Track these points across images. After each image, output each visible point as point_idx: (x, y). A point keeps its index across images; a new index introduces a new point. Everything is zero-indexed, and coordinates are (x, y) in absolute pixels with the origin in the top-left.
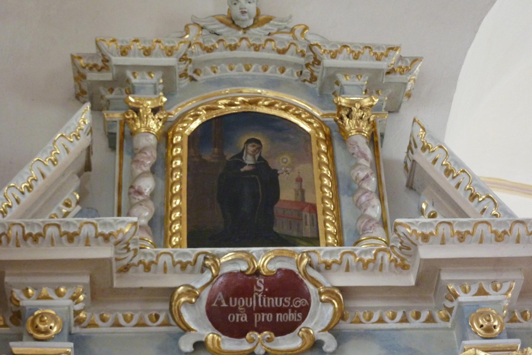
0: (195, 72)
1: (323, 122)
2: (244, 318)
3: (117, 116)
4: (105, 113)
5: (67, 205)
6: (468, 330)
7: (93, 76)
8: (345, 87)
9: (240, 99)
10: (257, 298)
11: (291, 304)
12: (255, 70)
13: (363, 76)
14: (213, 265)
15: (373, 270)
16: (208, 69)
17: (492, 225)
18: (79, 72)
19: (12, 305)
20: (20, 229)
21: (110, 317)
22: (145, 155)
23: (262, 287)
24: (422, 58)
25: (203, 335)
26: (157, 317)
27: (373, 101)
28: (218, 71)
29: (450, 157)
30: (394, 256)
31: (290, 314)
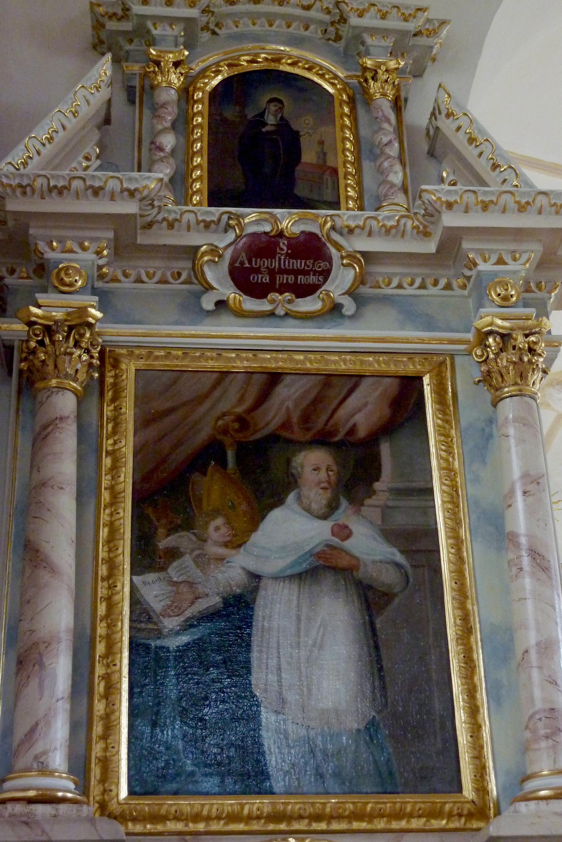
0: (217, 25)
1: (347, 83)
2: (266, 279)
3: (136, 68)
4: (124, 65)
5: (87, 159)
6: (486, 298)
7: (112, 25)
8: (371, 48)
9: (263, 56)
10: (280, 259)
11: (313, 266)
12: (279, 26)
13: (390, 37)
14: (237, 225)
15: (394, 236)
16: (230, 23)
17: (516, 194)
18: (97, 21)
19: (36, 258)
20: (46, 181)
21: (133, 273)
22: (166, 111)
23: (285, 248)
24: (450, 21)
25: (226, 295)
26: (179, 274)
27: (399, 64)
28: (241, 26)
29: (474, 125)
30: (416, 223)
31: (312, 277)
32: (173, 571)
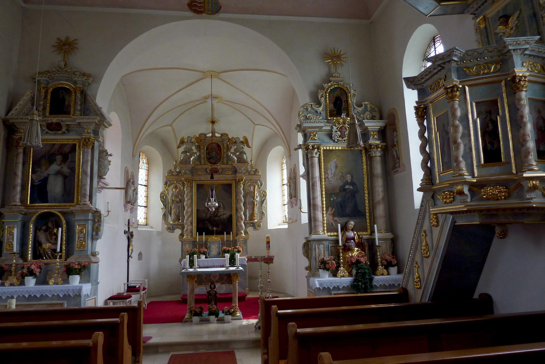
32: (37, 174)
